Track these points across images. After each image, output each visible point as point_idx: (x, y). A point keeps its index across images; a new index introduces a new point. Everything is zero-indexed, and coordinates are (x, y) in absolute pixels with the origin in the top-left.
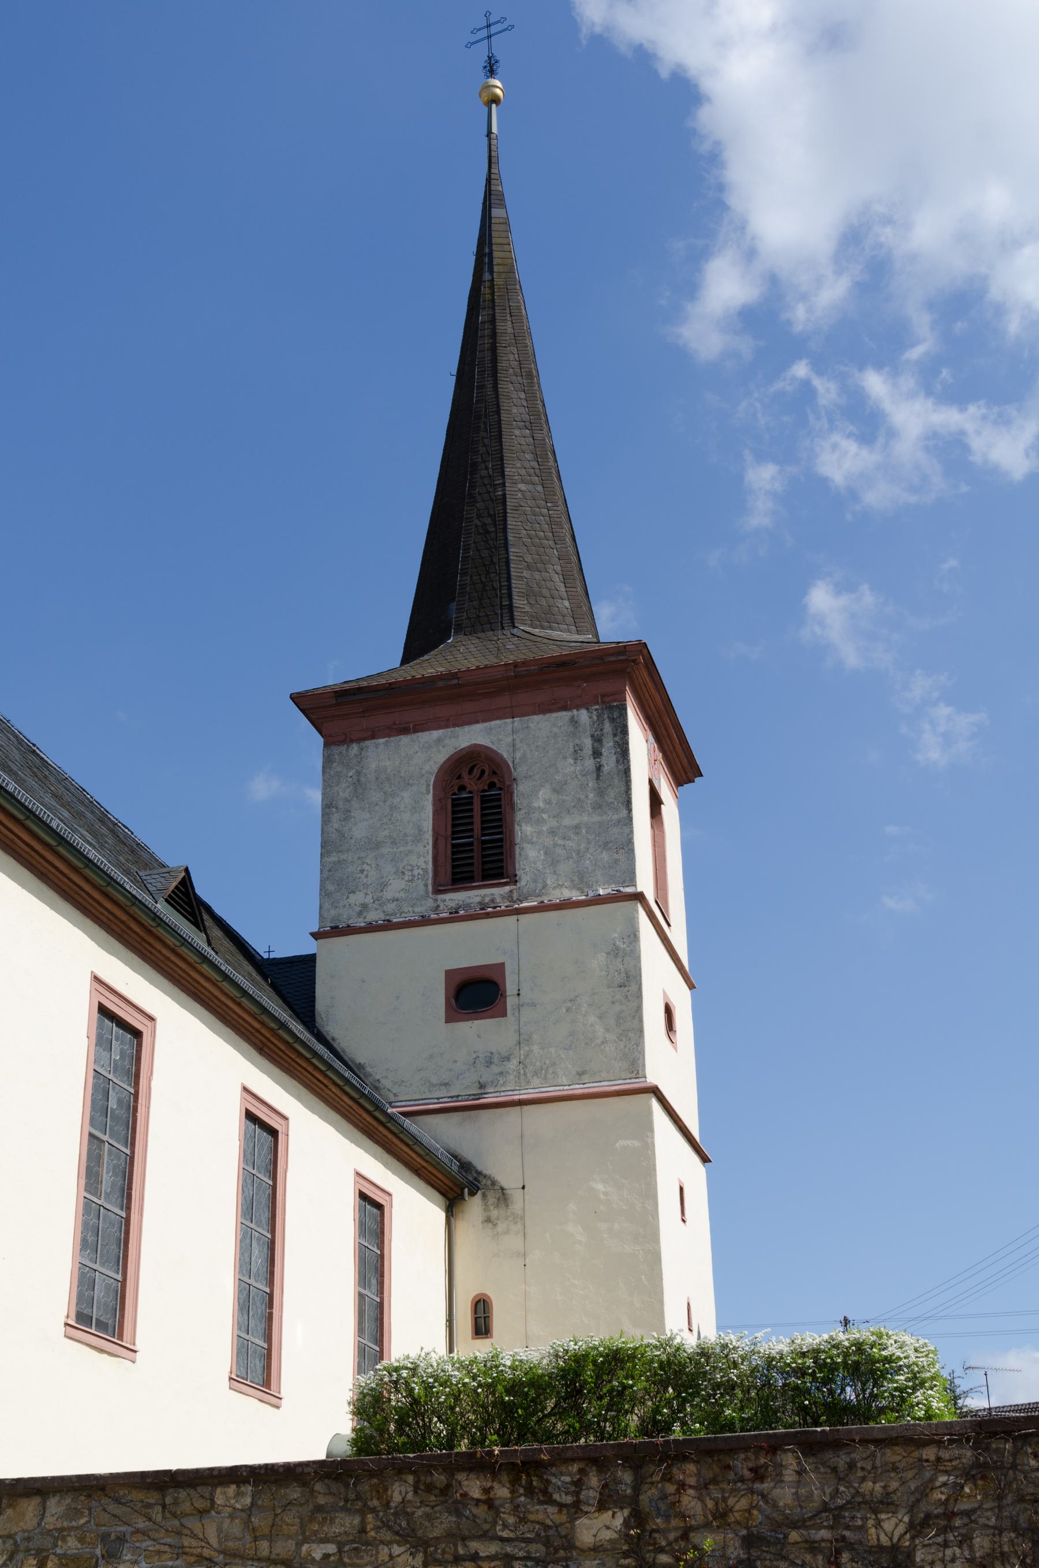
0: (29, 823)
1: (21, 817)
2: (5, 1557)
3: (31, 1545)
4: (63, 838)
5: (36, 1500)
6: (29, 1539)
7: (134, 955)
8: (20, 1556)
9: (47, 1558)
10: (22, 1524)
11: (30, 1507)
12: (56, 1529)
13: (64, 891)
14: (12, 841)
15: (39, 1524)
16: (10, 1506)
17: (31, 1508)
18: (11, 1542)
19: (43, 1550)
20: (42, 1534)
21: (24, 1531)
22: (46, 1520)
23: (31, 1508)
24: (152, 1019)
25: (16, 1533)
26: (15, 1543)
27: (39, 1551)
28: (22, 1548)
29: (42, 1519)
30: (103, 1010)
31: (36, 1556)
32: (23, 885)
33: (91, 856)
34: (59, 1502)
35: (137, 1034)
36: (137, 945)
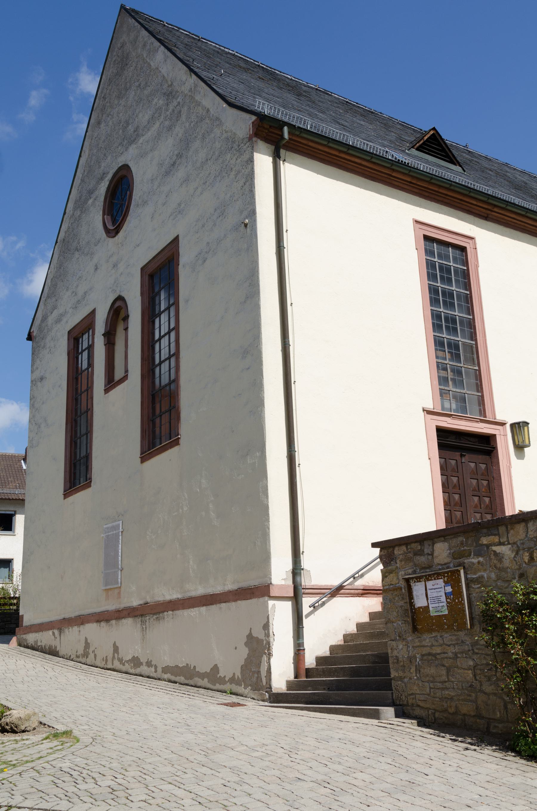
0: (509, 208)
1: (524, 213)
2: (514, 553)
3: (525, 546)
4: (372, 153)
5: (523, 524)
6: (523, 544)
7: (352, 175)
8: (521, 552)
9: (533, 551)
10: (518, 537)
11: (520, 528)
12: (534, 537)
13: (321, 158)
14: (525, 226)
15: (526, 536)
16: (512, 529)
17: (521, 529)
18: (516, 546)
19: (531, 548)
20: (529, 540)
21: (520, 540)
22: (529, 533)
23: (521, 529)
24: (472, 238)
25: (517, 542)
26: (518, 546)
27: (529, 549)
28: (521, 548)
29: (527, 533)
30: (426, 238)
31: (528, 551)
32: (420, 206)
33: (490, 193)
34: (533, 524)
35: (463, 249)
36: (327, 158)
